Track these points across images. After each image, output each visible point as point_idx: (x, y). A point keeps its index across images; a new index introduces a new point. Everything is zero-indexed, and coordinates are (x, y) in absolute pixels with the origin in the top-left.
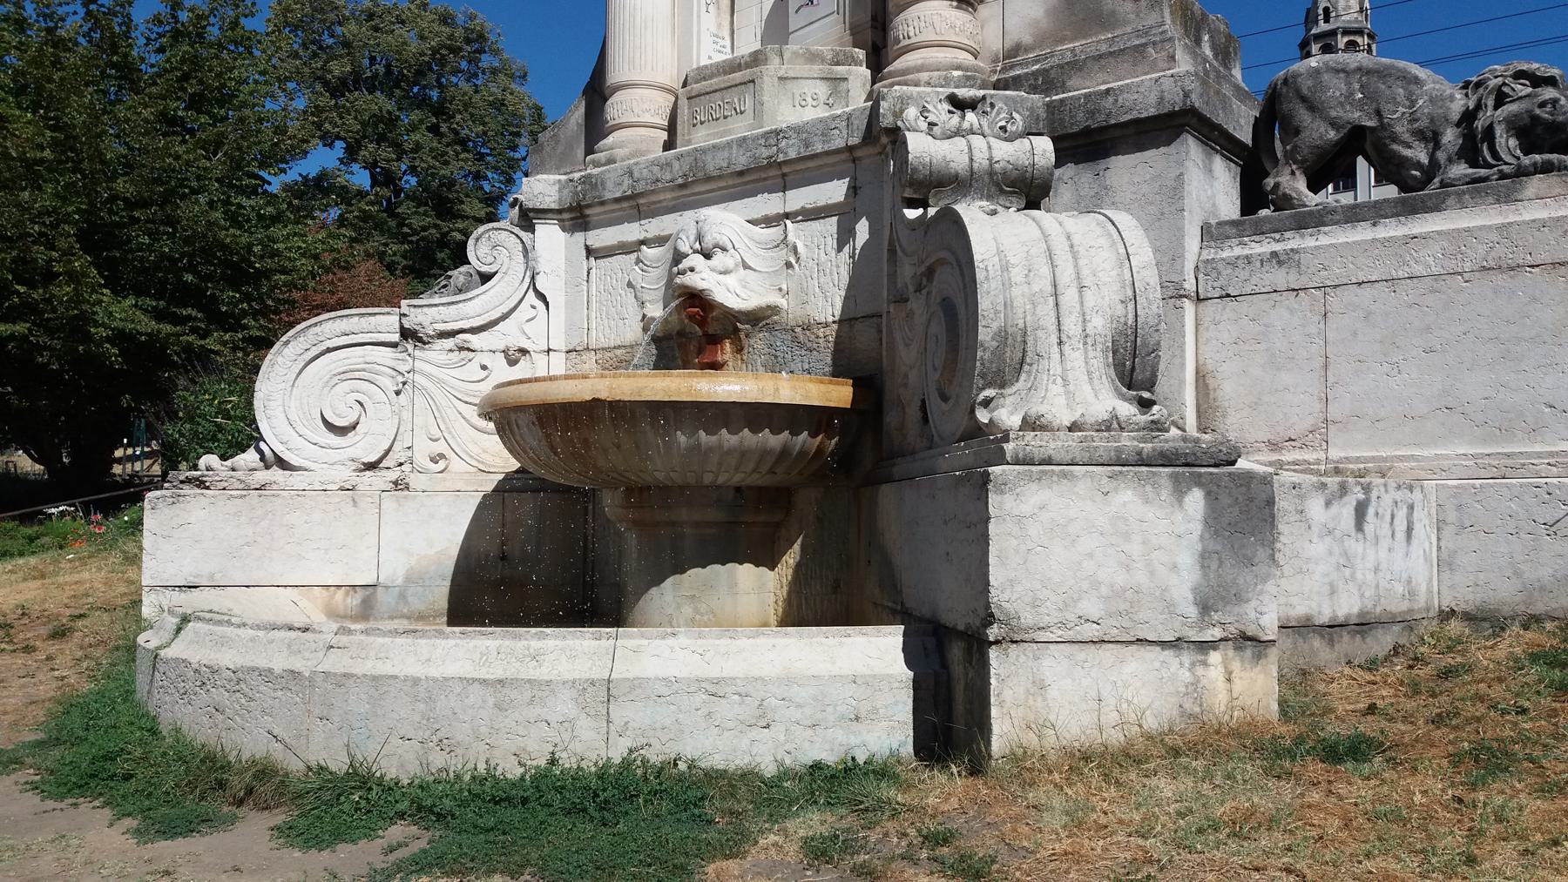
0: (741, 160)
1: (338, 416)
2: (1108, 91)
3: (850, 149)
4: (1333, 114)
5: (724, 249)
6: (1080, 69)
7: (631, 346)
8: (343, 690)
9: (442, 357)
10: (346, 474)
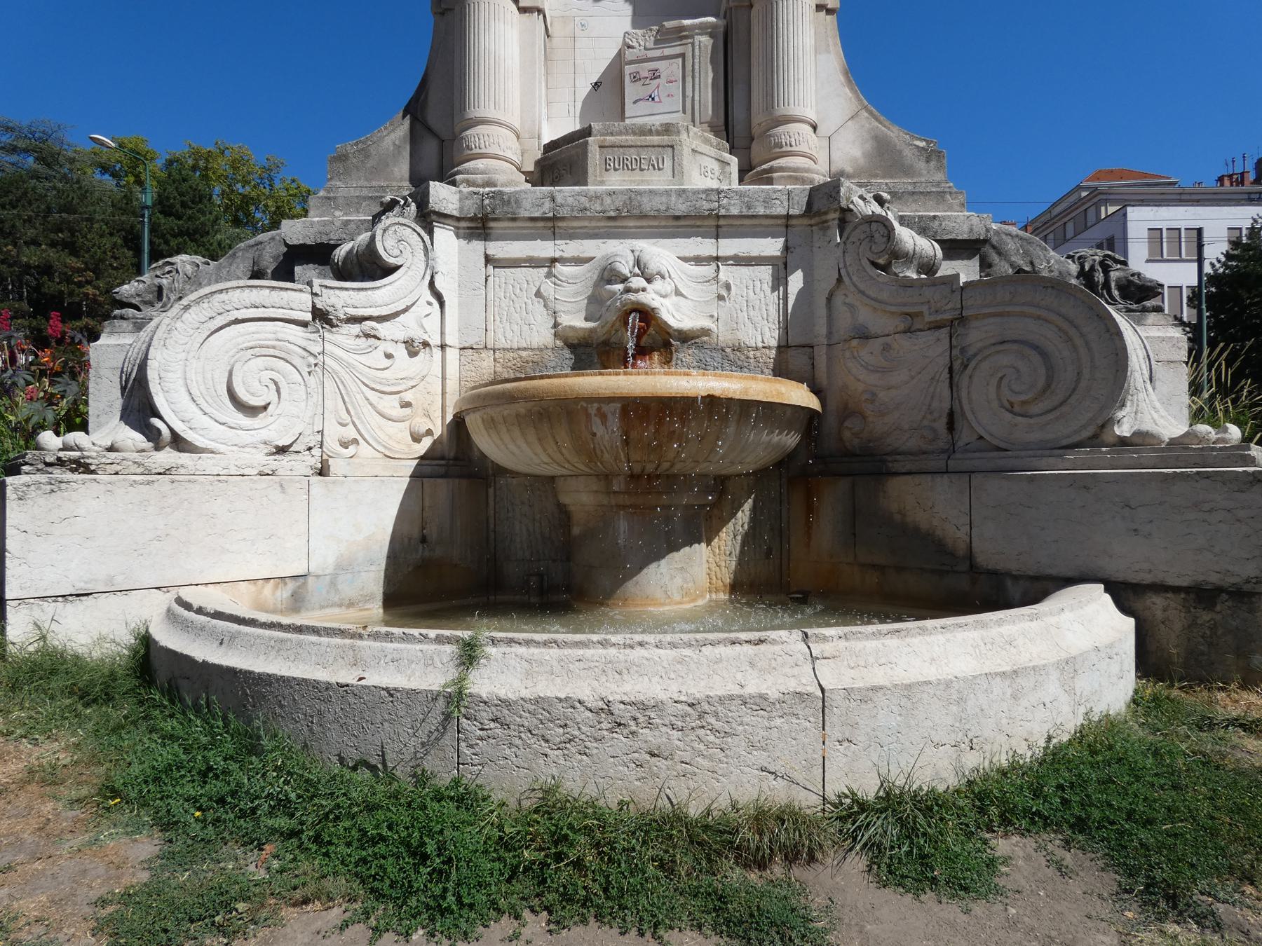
0: (681, 207)
1: (253, 394)
2: (935, 217)
3: (788, 217)
4: (1013, 259)
5: (663, 277)
6: (900, 198)
7: (540, 349)
8: (871, 705)
9: (351, 342)
10: (260, 458)
